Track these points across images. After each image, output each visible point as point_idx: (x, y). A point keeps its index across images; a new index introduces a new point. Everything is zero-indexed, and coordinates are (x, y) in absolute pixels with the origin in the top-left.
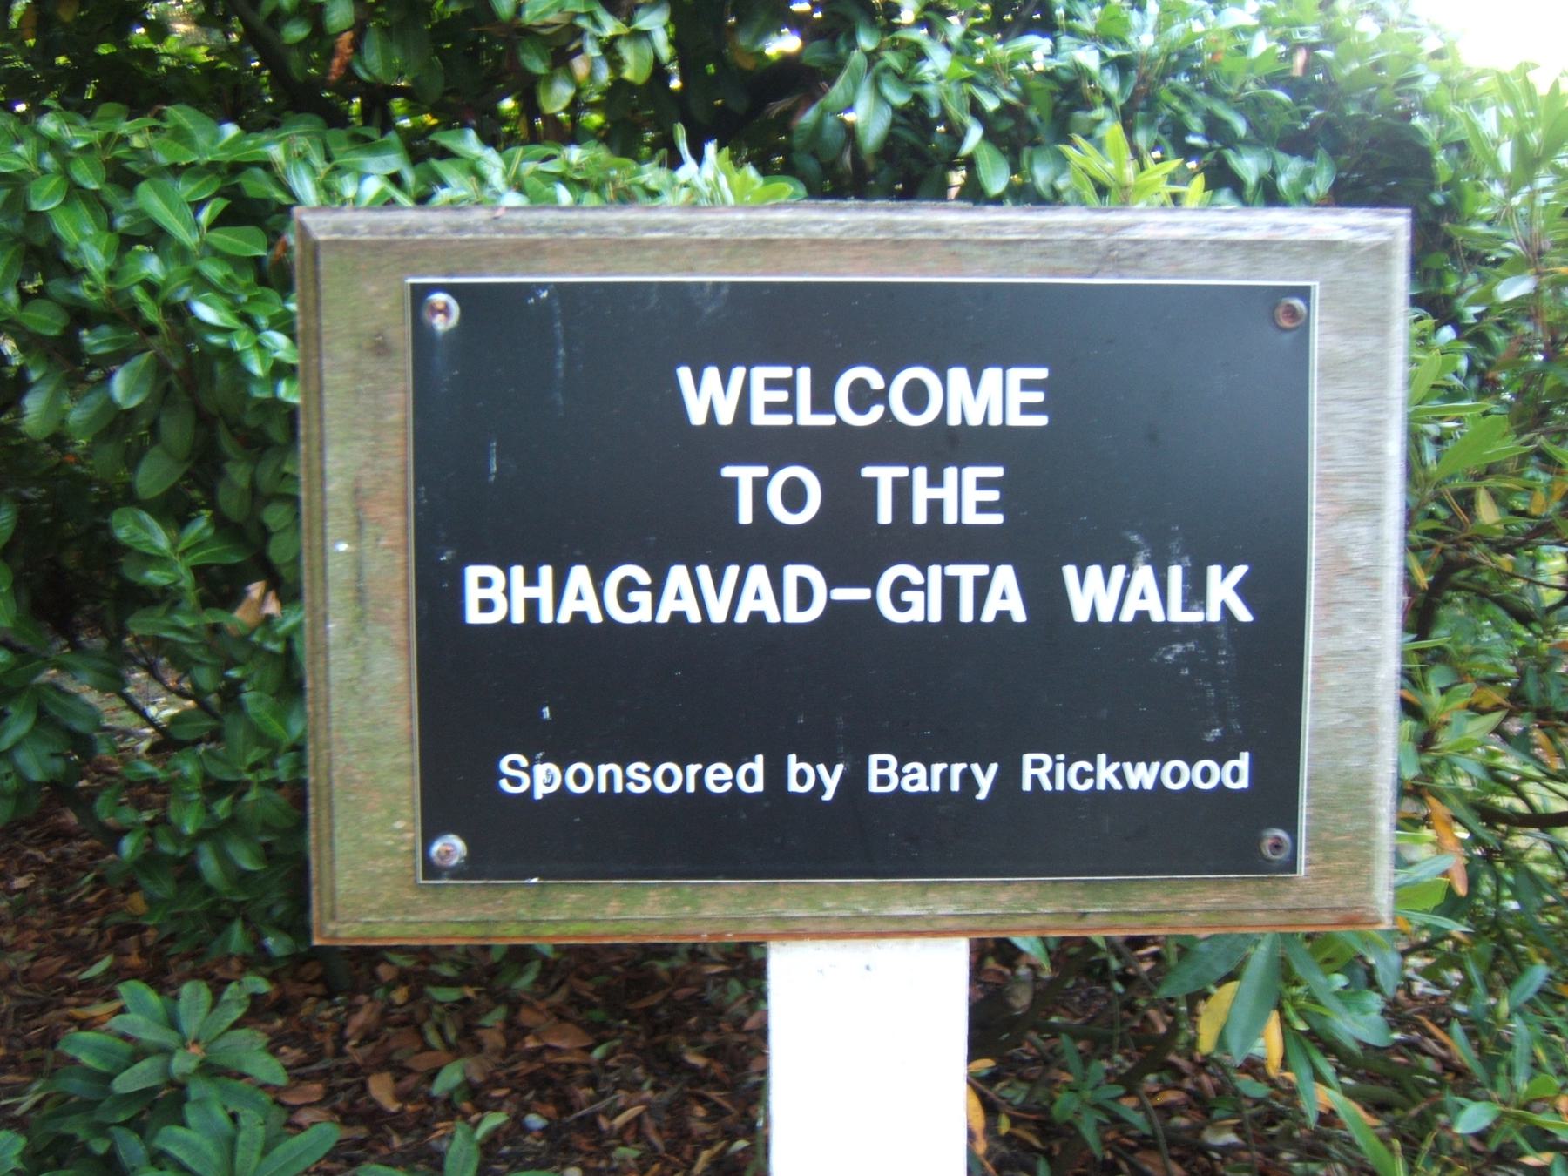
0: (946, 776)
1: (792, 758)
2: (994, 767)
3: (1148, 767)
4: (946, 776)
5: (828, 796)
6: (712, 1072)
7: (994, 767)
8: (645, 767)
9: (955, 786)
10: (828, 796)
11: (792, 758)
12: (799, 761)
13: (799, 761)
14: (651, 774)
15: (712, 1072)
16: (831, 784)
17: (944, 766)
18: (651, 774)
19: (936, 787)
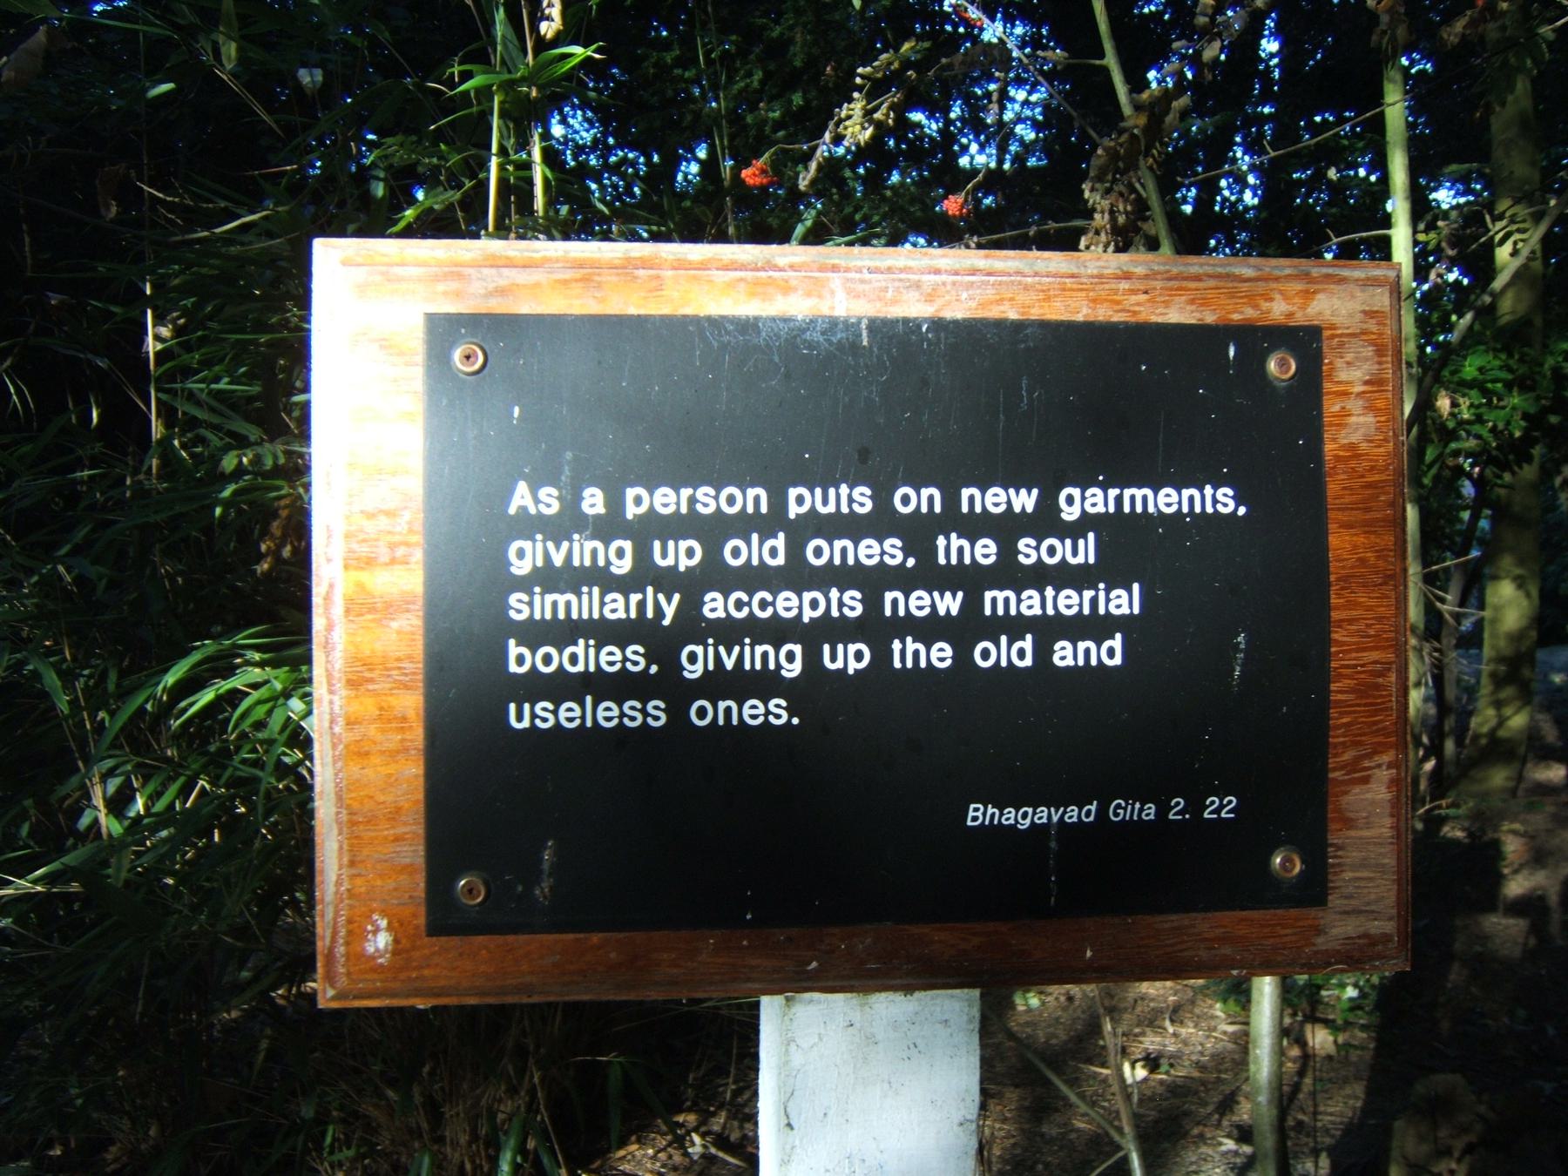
0: (1119, 499)
1: (512, 642)
2: (677, 597)
3: (1029, 493)
4: (1119, 499)
5: (666, 622)
6: (269, 463)
7: (677, 597)
8: (1033, 543)
9: (650, 614)
10: (666, 622)
11: (512, 642)
12: (518, 645)
13: (518, 645)
14: (1037, 548)
15: (269, 463)
16: (670, 611)
17: (1117, 491)
18: (1037, 548)
19: (1112, 509)
